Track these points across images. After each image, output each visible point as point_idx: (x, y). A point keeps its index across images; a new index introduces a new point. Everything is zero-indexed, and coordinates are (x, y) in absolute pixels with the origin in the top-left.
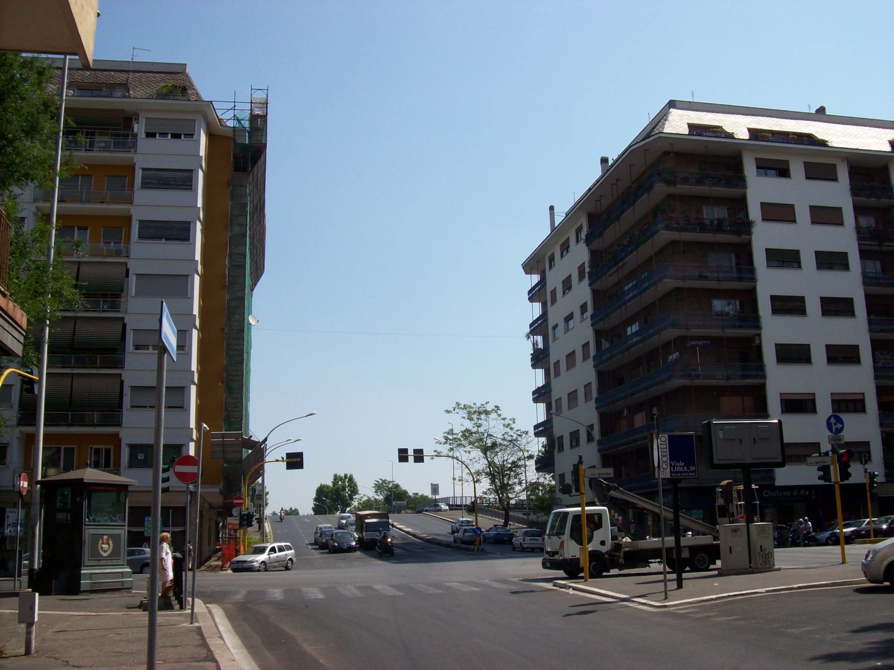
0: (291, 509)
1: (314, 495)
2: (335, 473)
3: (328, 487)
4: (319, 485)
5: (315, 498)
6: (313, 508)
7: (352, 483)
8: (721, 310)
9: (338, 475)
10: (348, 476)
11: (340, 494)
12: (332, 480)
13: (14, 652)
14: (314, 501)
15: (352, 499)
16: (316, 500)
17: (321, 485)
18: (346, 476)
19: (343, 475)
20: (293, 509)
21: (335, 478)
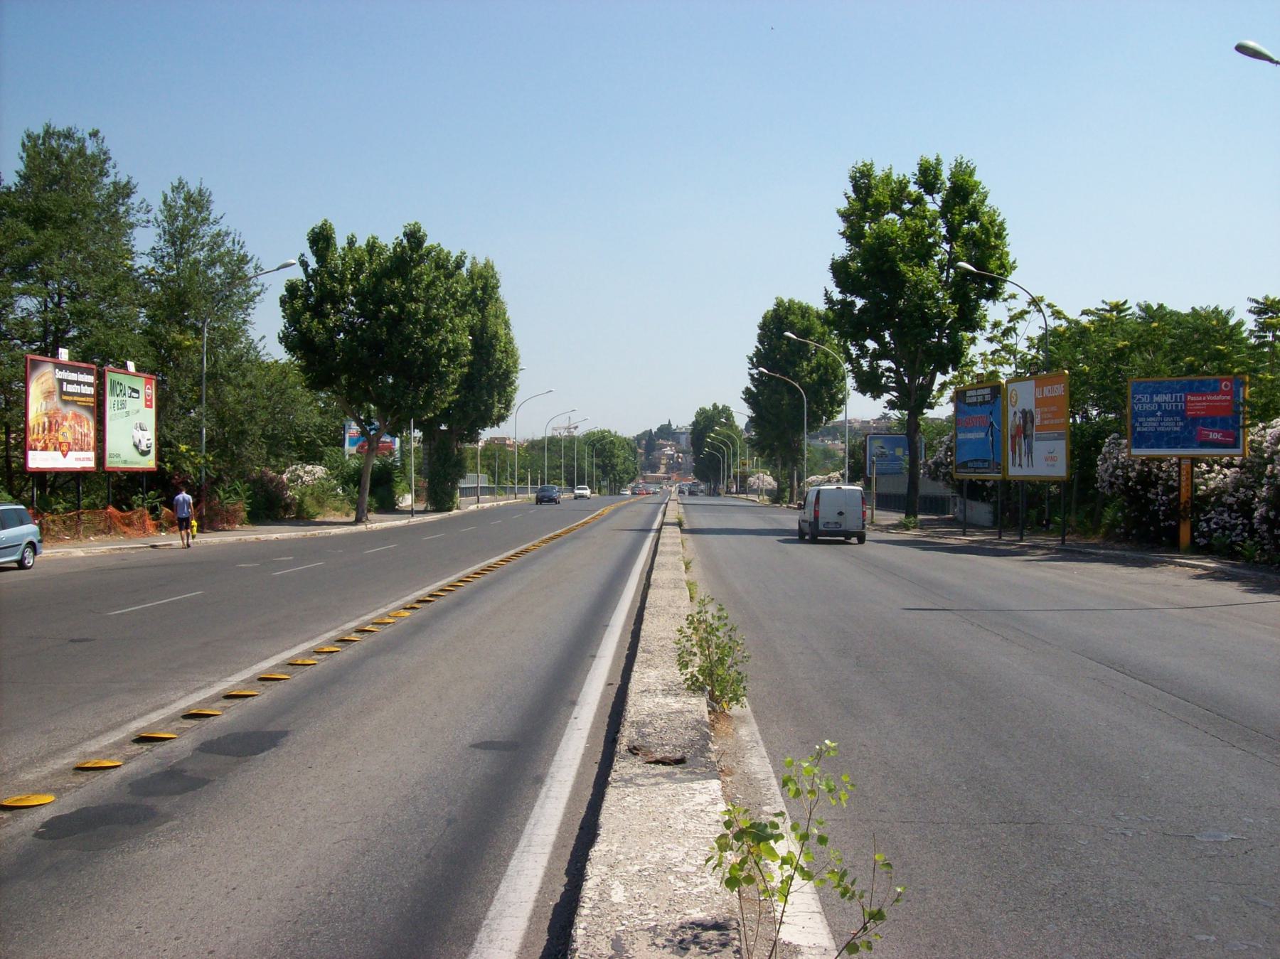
0: (715, 406)
1: (751, 344)
2: (858, 159)
3: (805, 311)
4: (771, 306)
5: (758, 353)
6: (748, 389)
7: (974, 215)
8: (1008, 279)
9: (878, 172)
10: (945, 174)
11: (900, 279)
12: (844, 205)
13: (149, 747)
14: (755, 366)
15: (970, 320)
16: (759, 359)
17: (780, 304)
18: (928, 177)
19: (906, 170)
20: (720, 408)
21: (856, 189)
